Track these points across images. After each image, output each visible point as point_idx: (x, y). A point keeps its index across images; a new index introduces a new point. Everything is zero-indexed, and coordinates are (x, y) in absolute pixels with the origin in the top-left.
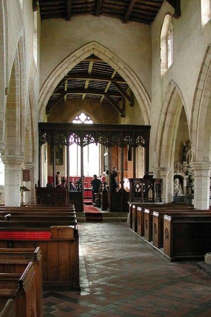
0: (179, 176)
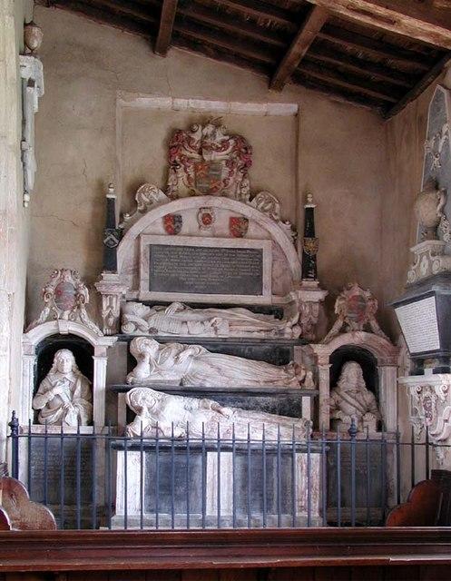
0: (71, 336)
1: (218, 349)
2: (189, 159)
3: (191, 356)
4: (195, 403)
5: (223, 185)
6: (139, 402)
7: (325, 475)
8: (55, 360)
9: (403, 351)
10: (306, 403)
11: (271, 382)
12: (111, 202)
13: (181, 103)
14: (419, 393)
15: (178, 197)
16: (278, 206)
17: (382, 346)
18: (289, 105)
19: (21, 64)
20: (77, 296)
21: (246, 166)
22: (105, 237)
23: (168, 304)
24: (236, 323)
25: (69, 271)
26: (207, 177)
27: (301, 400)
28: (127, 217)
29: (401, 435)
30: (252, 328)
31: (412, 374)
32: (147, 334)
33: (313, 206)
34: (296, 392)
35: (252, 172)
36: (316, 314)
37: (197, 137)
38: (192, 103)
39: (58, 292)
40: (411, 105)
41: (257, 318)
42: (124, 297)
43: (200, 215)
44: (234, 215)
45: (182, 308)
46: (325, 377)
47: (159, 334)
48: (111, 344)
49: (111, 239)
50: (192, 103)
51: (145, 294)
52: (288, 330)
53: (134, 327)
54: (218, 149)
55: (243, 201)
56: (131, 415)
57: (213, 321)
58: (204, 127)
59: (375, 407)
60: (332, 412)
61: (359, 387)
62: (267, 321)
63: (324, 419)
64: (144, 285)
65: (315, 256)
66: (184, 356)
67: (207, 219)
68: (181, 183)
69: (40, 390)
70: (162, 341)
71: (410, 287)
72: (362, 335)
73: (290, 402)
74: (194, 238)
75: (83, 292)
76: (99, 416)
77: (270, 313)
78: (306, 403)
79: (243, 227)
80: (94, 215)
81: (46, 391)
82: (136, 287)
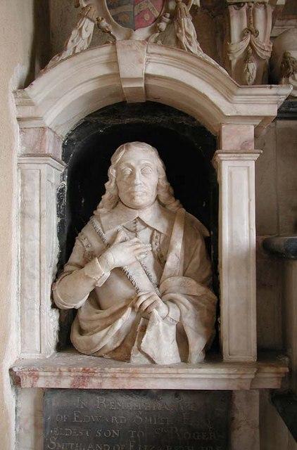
8: (112, 172)
69: (75, 257)
81: (89, 258)
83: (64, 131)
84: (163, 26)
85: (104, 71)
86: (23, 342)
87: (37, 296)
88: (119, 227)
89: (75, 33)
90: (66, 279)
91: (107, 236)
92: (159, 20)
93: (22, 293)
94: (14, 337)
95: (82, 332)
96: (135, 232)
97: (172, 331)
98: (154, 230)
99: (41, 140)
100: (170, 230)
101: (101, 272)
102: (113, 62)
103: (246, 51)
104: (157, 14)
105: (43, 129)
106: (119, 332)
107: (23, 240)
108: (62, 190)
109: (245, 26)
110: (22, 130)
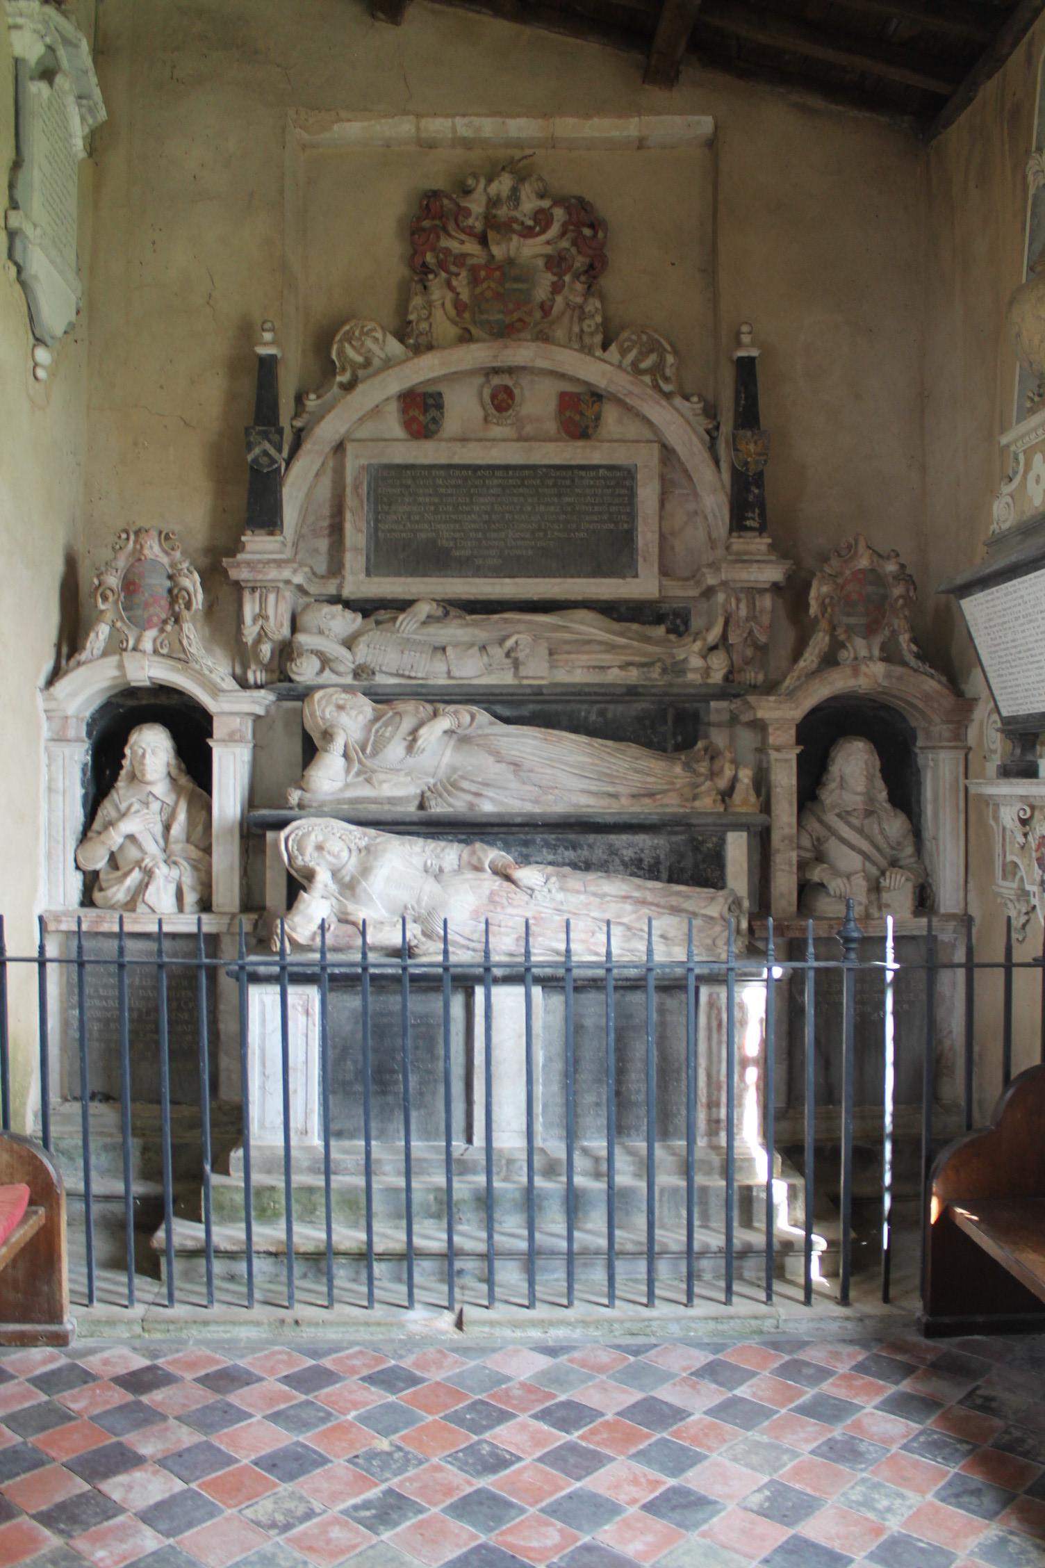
0: (162, 690)
1: (525, 711)
2: (461, 259)
3: (449, 733)
4: (450, 854)
5: (538, 314)
6: (308, 858)
7: (785, 1027)
8: (127, 751)
9: (981, 712)
10: (737, 848)
11: (651, 795)
12: (267, 368)
13: (438, 126)
14: (1024, 822)
15: (430, 347)
16: (670, 359)
17: (927, 697)
18: (690, 118)
19: (10, 21)
20: (173, 595)
21: (594, 271)
22: (249, 447)
23: (403, 605)
24: (567, 647)
25: (154, 533)
26: (498, 296)
27: (722, 842)
28: (312, 402)
29: (977, 922)
30: (606, 659)
31: (1006, 772)
32: (349, 680)
33: (754, 353)
34: (710, 820)
35: (610, 282)
36: (766, 619)
37: (476, 205)
38: (463, 126)
39: (130, 586)
40: (989, 89)
41: (621, 634)
42: (301, 589)
43: (487, 392)
44: (569, 388)
45: (440, 612)
46: (785, 779)
47: (380, 679)
48: (260, 711)
49: (266, 453)
50: (463, 126)
51: (357, 583)
52: (696, 662)
53: (316, 663)
54: (528, 233)
55: (586, 350)
56: (296, 885)
57: (510, 643)
58: (490, 181)
59: (909, 850)
60: (802, 866)
61: (871, 800)
62: (647, 639)
63: (784, 883)
64: (354, 562)
65: (760, 475)
66: (433, 734)
67: (502, 401)
68: (438, 314)
69: (97, 825)
70: (381, 698)
71: (998, 542)
72: (879, 669)
73: (695, 845)
74: (471, 445)
75: (186, 582)
76: (227, 892)
77: (659, 619)
78: (737, 848)
79: (590, 413)
80: (231, 397)
81: (110, 824)
82: (336, 568)
83: (87, 714)
84: (169, 628)
85: (115, 673)
86: (50, 896)
87: (61, 859)
88: (134, 800)
89: (92, 635)
90: (88, 846)
91: (123, 807)
92: (165, 622)
93: (49, 855)
94: (42, 890)
95: (101, 889)
96: (146, 804)
97: (172, 888)
98: (163, 802)
99: (64, 727)
100: (176, 803)
101: (115, 838)
102: (121, 666)
103: (259, 634)
104: (164, 616)
105: (67, 718)
106: (129, 889)
107: (50, 811)
108: (86, 765)
109: (257, 610)
110: (48, 718)
